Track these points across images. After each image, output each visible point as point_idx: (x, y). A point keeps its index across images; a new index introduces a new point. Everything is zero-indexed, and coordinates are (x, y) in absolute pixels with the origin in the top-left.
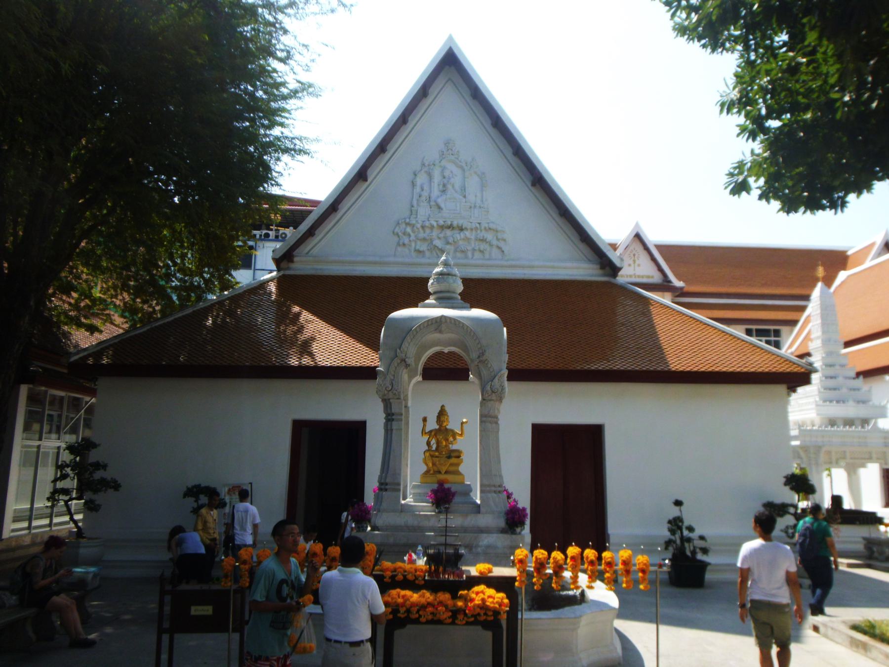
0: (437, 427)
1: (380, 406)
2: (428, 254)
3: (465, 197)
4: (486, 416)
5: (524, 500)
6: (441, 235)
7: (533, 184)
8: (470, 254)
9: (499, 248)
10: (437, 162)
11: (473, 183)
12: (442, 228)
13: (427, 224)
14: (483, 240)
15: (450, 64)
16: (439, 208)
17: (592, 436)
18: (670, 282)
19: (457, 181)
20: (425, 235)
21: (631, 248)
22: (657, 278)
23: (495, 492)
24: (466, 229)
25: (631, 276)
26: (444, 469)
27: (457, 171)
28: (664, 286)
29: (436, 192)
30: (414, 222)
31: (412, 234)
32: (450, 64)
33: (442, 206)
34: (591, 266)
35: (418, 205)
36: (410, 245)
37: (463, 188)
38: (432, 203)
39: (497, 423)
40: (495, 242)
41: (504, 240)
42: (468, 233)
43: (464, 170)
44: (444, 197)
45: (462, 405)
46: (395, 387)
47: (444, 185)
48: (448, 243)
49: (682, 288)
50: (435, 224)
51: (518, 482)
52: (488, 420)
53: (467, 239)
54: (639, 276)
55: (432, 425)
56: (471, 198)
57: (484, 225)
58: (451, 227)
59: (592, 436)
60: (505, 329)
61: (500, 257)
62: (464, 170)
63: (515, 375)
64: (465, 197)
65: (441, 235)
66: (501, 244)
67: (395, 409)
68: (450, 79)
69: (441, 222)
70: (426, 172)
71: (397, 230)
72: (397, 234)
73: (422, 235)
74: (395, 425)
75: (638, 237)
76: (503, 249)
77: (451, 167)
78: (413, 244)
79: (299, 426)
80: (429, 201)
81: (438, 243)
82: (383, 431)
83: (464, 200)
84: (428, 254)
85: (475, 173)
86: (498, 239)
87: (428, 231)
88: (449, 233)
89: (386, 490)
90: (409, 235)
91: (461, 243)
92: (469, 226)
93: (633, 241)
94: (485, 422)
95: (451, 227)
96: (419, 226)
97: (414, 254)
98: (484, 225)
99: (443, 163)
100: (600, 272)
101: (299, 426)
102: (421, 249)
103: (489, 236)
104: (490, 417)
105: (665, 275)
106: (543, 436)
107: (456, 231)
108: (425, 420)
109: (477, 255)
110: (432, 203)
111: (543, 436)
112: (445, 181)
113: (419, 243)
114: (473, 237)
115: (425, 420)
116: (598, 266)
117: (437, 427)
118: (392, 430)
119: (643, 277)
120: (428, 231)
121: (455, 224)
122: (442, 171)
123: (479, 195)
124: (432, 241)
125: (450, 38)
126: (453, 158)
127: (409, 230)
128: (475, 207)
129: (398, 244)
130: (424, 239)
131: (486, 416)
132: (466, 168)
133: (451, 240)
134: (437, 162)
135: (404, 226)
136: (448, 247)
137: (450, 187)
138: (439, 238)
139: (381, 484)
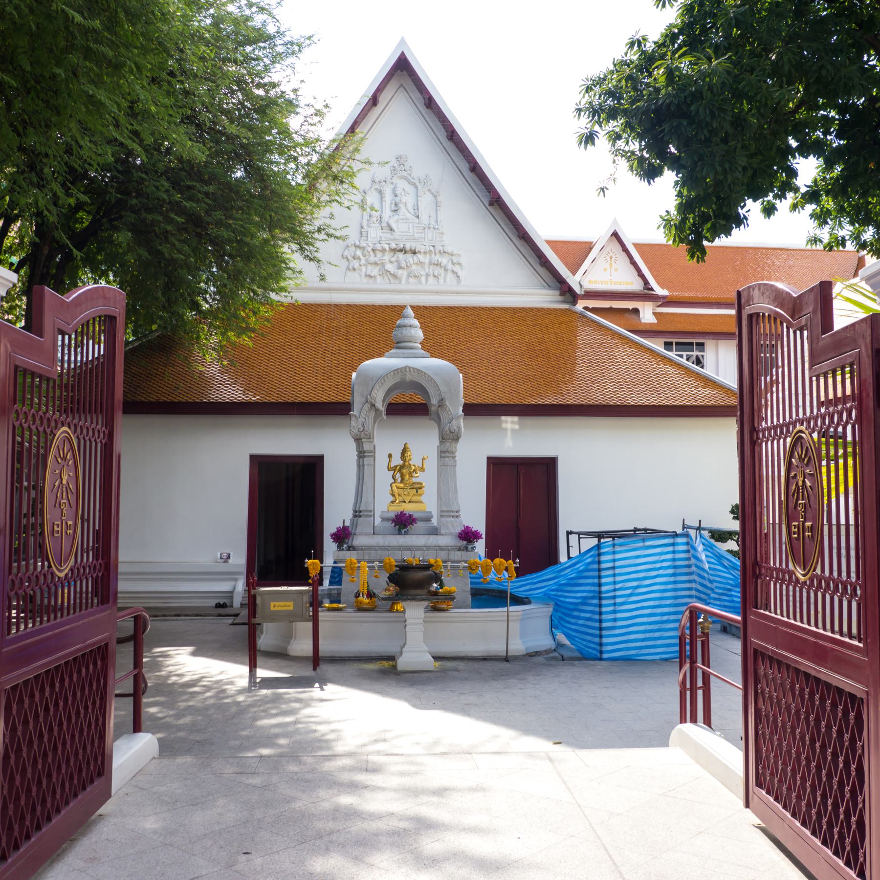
0: (401, 462)
1: (353, 445)
2: (379, 279)
3: (418, 217)
4: (444, 452)
5: (479, 524)
6: (393, 259)
7: (491, 204)
8: (423, 279)
9: (453, 272)
10: (389, 179)
11: (426, 200)
12: (394, 251)
13: (378, 247)
14: (438, 264)
15: (402, 68)
16: (391, 229)
17: (547, 467)
18: (652, 289)
19: (409, 200)
20: (376, 259)
21: (607, 249)
22: (636, 285)
23: (453, 517)
24: (420, 252)
25: (606, 283)
26: (407, 499)
27: (410, 189)
28: (646, 295)
29: (387, 214)
30: (365, 245)
31: (362, 257)
32: (402, 68)
33: (394, 226)
34: (550, 292)
35: (368, 226)
36: (361, 270)
37: (416, 208)
38: (384, 224)
39: (454, 457)
40: (450, 266)
41: (459, 264)
42: (421, 257)
43: (416, 187)
44: (396, 217)
45: (422, 442)
46: (366, 428)
47: (396, 205)
48: (400, 268)
49: (664, 297)
50: (387, 247)
51: (474, 513)
52: (446, 454)
53: (421, 263)
54: (615, 283)
55: (397, 461)
56: (424, 218)
57: (439, 247)
58: (403, 250)
59: (547, 467)
60: (461, 375)
61: (455, 283)
62: (416, 187)
63: (471, 410)
64: (418, 217)
65: (393, 259)
66: (457, 268)
67: (366, 447)
68: (402, 85)
69: (393, 246)
70: (376, 189)
71: (346, 253)
72: (347, 258)
73: (372, 259)
74: (367, 461)
75: (615, 235)
76: (459, 274)
77: (402, 185)
78: (364, 268)
79: (254, 458)
80: (381, 222)
81: (390, 267)
82: (356, 467)
83: (417, 220)
84: (379, 279)
85: (429, 190)
86: (453, 264)
87: (379, 254)
88: (401, 255)
89: (360, 516)
90: (359, 258)
91: (414, 267)
92: (423, 249)
93: (609, 240)
94: (444, 457)
95: (403, 250)
96: (370, 249)
97: (365, 280)
98: (439, 247)
99: (395, 180)
100: (560, 298)
101: (254, 458)
102: (372, 274)
103: (444, 260)
104: (449, 453)
105: (646, 283)
106: (498, 467)
107: (409, 256)
108: (390, 456)
109: (431, 280)
110: (384, 224)
111: (498, 467)
112: (397, 199)
113: (370, 267)
114: (427, 261)
115: (390, 456)
116: (558, 292)
117: (401, 462)
118: (364, 465)
119: (620, 283)
120: (379, 254)
121: (408, 247)
122: (394, 190)
123: (433, 215)
124: (383, 265)
125: (402, 41)
126: (405, 174)
127: (359, 253)
128: (429, 228)
129: (348, 269)
130: (376, 264)
131: (444, 452)
132: (418, 184)
133: (403, 264)
134: (389, 179)
135: (354, 248)
136: (400, 272)
137: (402, 206)
138: (391, 262)
139: (355, 511)
